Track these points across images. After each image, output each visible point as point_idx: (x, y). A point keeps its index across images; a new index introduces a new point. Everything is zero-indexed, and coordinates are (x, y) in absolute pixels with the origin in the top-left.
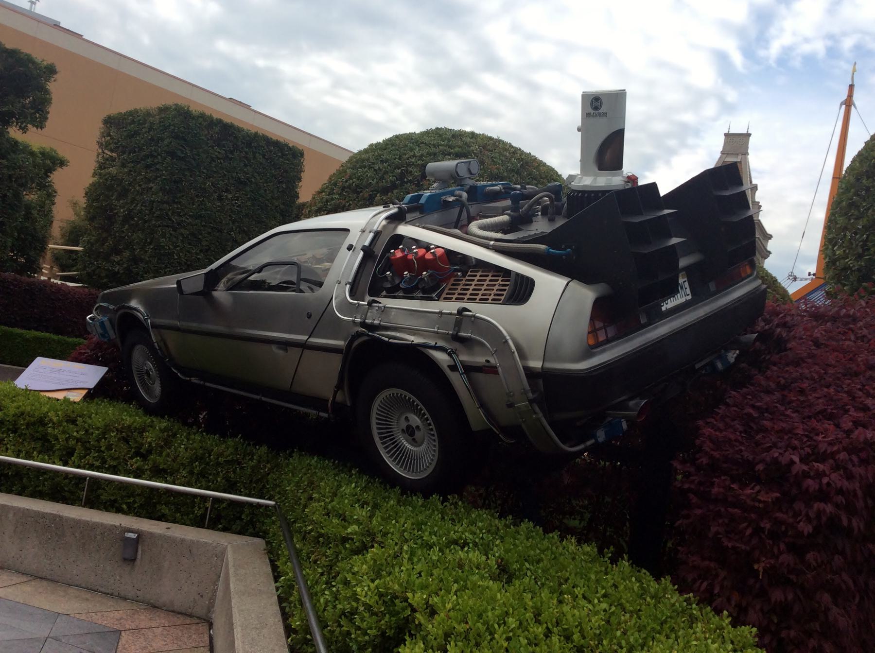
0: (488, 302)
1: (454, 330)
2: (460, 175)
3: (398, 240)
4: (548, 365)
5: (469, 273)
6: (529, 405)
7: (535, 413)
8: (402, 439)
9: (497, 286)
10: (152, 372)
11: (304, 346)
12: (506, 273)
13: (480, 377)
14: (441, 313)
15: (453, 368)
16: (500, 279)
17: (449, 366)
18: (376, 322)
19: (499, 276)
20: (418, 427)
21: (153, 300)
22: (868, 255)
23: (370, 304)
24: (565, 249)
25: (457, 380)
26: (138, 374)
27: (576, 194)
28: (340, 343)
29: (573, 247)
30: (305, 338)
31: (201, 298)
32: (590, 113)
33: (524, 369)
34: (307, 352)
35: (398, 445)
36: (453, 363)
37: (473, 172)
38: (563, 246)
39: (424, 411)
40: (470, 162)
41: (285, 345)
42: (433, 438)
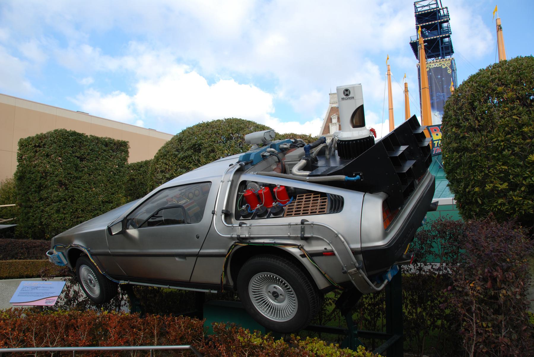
1: (301, 234)
2: (267, 139)
3: (244, 184)
4: (364, 245)
5: (297, 198)
7: (361, 274)
8: (268, 298)
11: (198, 255)
12: (323, 195)
13: (315, 258)
14: (290, 225)
15: (303, 256)
16: (305, 195)
18: (247, 236)
19: (318, 197)
21: (86, 237)
24: (355, 176)
25: (306, 261)
28: (223, 251)
29: (361, 174)
30: (197, 250)
32: (344, 98)
33: (353, 253)
35: (272, 307)
36: (302, 253)
37: (273, 137)
38: (354, 175)
39: (281, 279)
40: (270, 131)
41: (184, 256)
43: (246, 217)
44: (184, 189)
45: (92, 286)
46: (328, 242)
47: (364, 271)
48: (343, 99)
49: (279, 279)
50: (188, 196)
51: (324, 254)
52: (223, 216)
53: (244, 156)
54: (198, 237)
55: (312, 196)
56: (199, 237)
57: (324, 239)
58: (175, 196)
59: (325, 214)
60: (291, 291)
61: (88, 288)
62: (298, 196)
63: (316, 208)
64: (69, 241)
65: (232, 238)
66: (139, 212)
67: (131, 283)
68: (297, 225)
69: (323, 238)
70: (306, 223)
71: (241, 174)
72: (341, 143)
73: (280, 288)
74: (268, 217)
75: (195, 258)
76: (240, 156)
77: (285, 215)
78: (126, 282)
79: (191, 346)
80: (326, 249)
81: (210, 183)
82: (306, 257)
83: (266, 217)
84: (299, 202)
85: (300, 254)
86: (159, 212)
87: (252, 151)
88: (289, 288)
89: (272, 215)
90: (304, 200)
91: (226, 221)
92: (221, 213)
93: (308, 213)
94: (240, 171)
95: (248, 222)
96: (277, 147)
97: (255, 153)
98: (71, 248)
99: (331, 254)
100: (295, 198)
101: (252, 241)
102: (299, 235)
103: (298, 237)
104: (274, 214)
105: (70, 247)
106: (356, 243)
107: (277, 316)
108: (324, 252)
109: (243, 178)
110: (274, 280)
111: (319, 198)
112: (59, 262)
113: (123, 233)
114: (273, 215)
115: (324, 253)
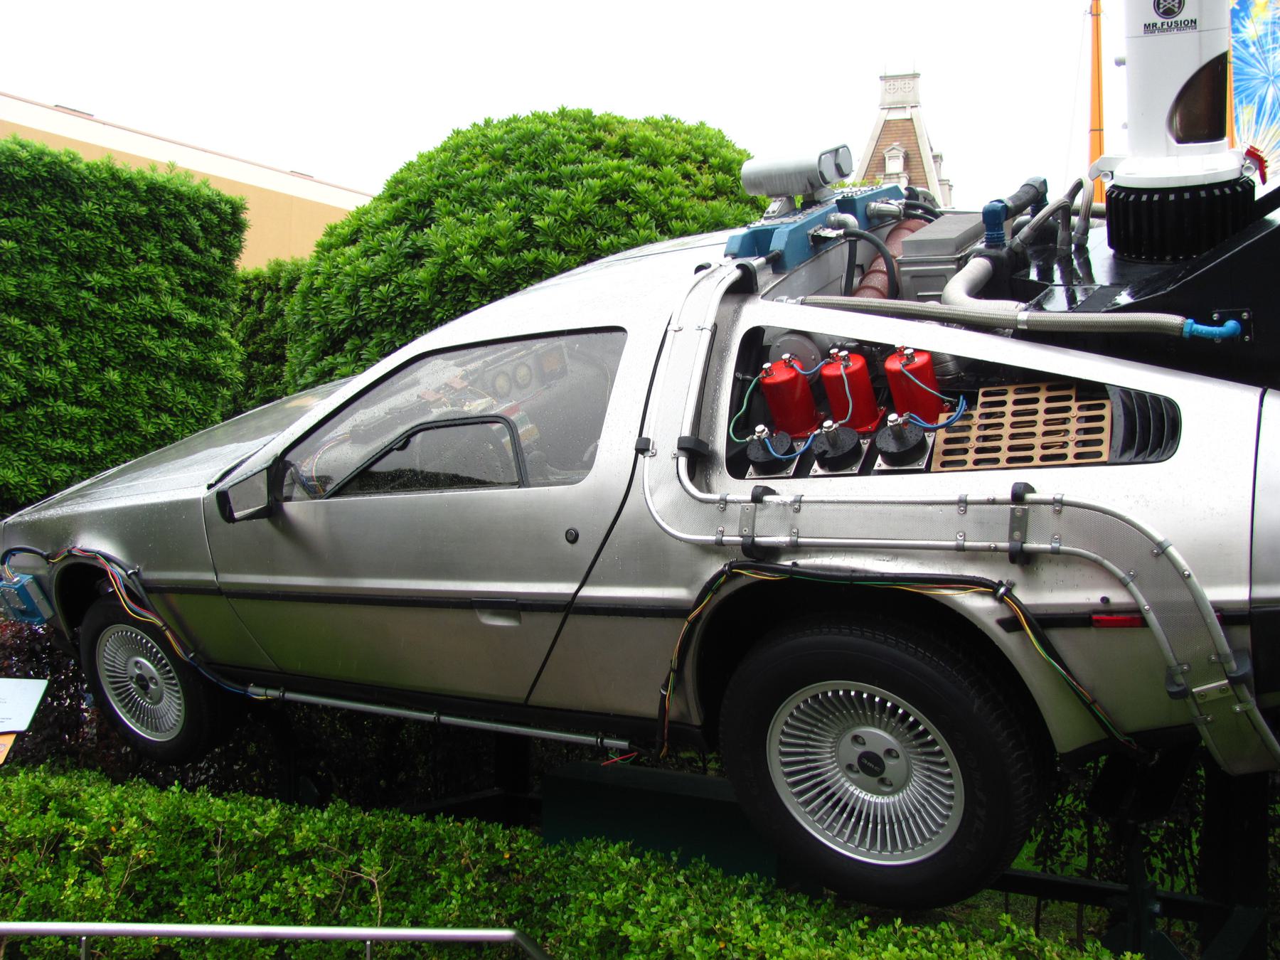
0: (965, 468)
1: (1011, 538)
3: (755, 344)
4: (1263, 592)
5: (981, 399)
6: (1229, 687)
9: (1073, 421)
10: (156, 684)
11: (569, 607)
12: (1091, 391)
13: (1058, 637)
14: (963, 503)
15: (1010, 624)
16: (1011, 389)
17: (1001, 622)
19: (1068, 398)
20: (889, 752)
22: (491, 370)
23: (757, 498)
24: (1220, 323)
26: (116, 689)
27: (1123, 194)
29: (1245, 315)
30: (567, 588)
31: (264, 523)
32: (1155, 25)
33: (1213, 607)
34: (574, 621)
36: (1006, 614)
38: (1215, 317)
42: (176, 689)
43: (771, 468)
44: (480, 357)
45: (146, 703)
46: (1121, 574)
47: (1251, 692)
48: (1149, 28)
49: (895, 708)
50: (493, 386)
51: (1098, 621)
52: (683, 461)
53: (745, 237)
54: (571, 539)
55: (1042, 395)
56: (577, 536)
57: (1106, 562)
58: (446, 385)
59: (1104, 464)
60: (940, 753)
61: (133, 717)
62: (981, 391)
63: (1064, 439)
64: (66, 528)
65: (717, 548)
66: (326, 438)
67: (290, 696)
68: (993, 502)
69: (1100, 558)
70: (1029, 496)
71: (744, 301)
72: (1132, 198)
73: (878, 737)
74: (866, 470)
75: (556, 619)
76: (732, 238)
77: (935, 466)
78: (273, 693)
79: (517, 935)
80: (1105, 600)
81: (620, 334)
82: (1021, 628)
83: (856, 470)
84: (988, 416)
85: (1000, 616)
86: (412, 439)
87: (778, 221)
88: (934, 742)
89: (879, 460)
90: (1009, 408)
91: (692, 477)
92: (676, 451)
93: (1030, 459)
94: (743, 288)
95: (786, 489)
96: (860, 208)
97: (792, 227)
98: (72, 561)
99: (1132, 618)
100: (972, 402)
101: (803, 562)
102: (1004, 545)
103: (996, 549)
104: (889, 458)
105: (66, 557)
106: (1227, 579)
107: (840, 832)
108: (1096, 612)
109: (756, 313)
110: (855, 708)
111: (1074, 404)
112: (23, 612)
113: (273, 512)
114: (822, 466)
115: (1095, 616)
